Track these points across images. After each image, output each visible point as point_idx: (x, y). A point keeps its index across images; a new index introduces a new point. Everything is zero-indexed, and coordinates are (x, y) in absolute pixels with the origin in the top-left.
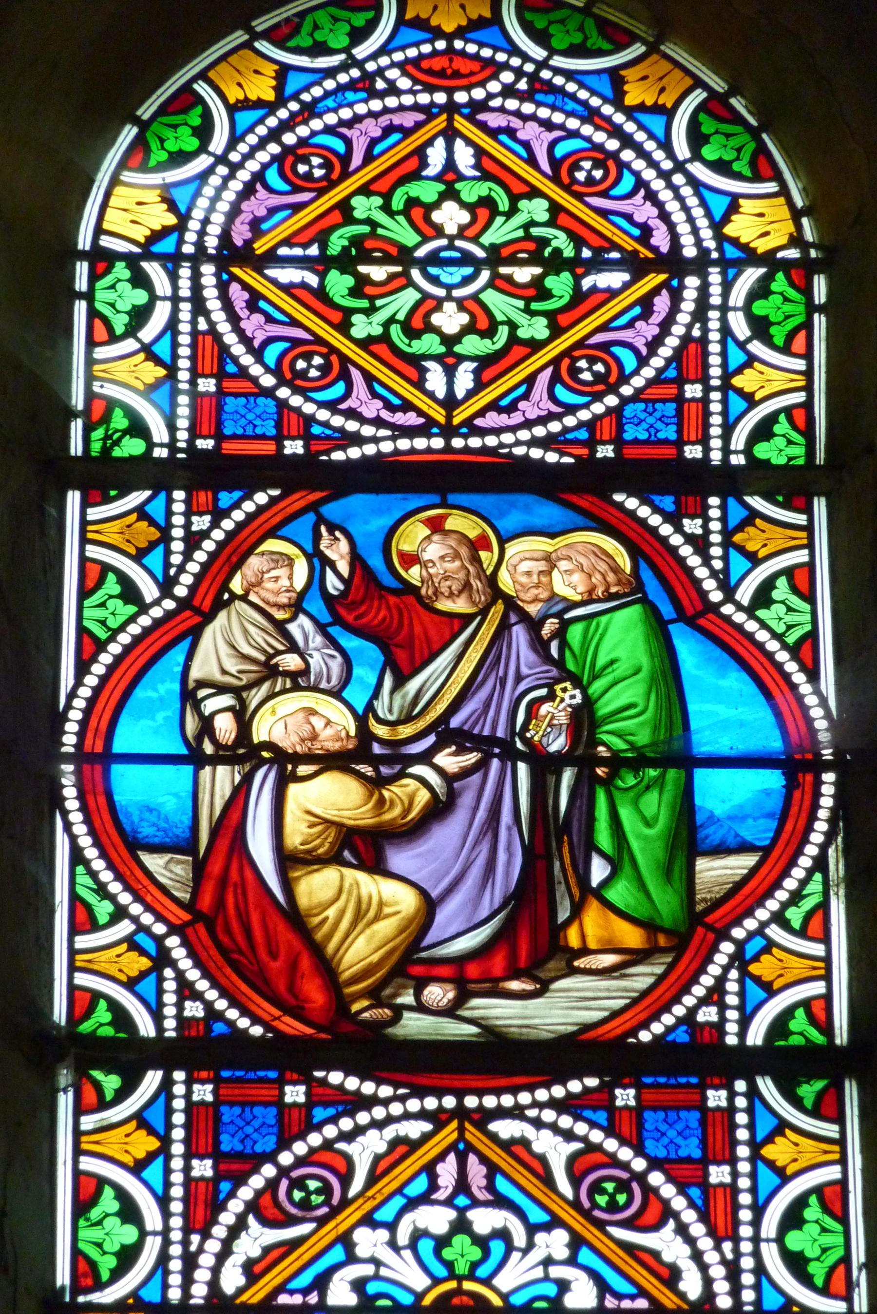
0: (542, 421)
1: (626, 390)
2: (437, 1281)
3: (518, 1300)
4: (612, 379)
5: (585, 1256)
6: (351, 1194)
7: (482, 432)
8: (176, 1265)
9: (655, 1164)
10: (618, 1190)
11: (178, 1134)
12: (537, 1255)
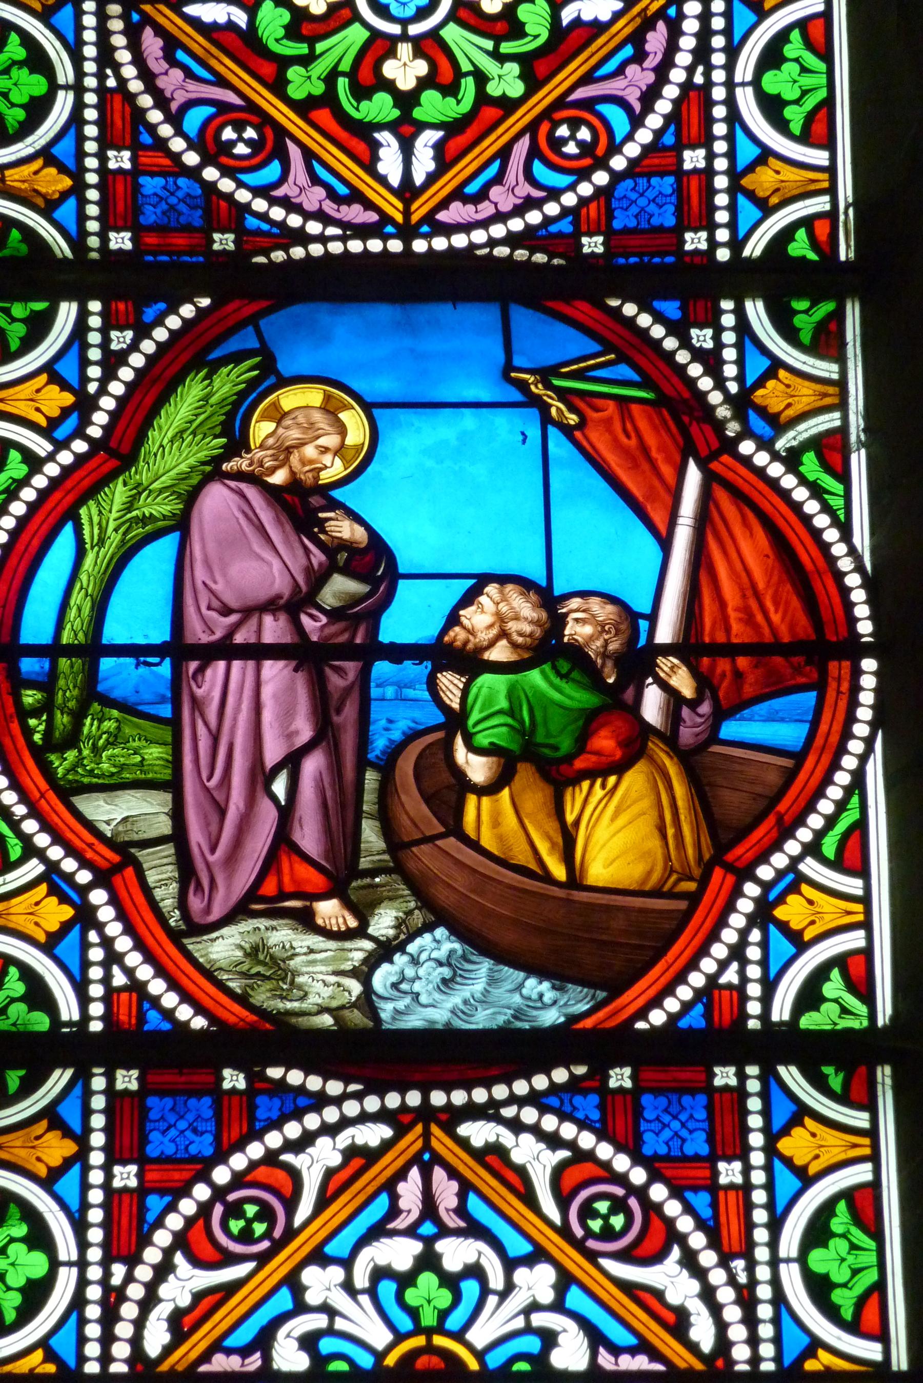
0: (519, 211)
1: (618, 163)
2: (399, 1337)
3: (495, 1360)
4: (600, 150)
5: (575, 1298)
6: (298, 1220)
7: (448, 230)
8: (93, 1312)
9: (194, 173)
10: (613, 1211)
11: (98, 1139)
12: (517, 1301)
